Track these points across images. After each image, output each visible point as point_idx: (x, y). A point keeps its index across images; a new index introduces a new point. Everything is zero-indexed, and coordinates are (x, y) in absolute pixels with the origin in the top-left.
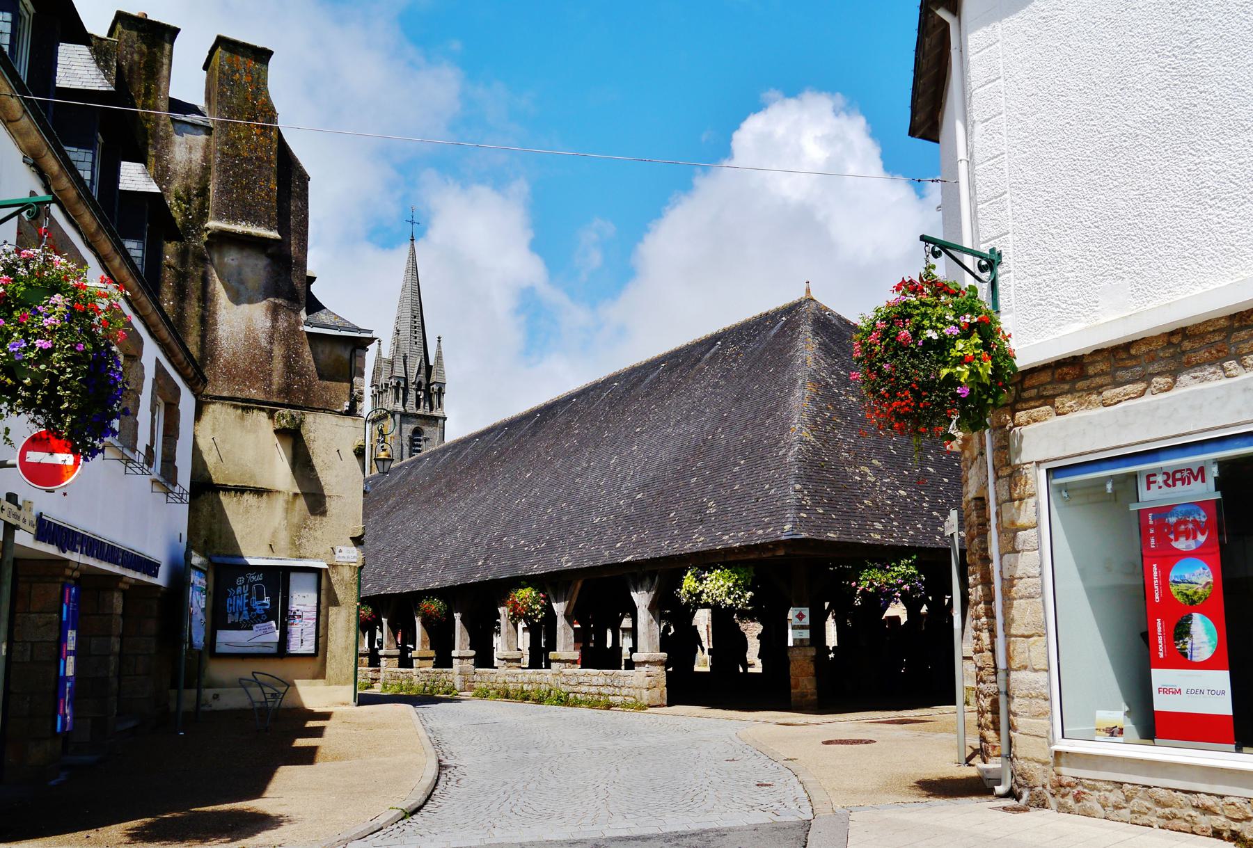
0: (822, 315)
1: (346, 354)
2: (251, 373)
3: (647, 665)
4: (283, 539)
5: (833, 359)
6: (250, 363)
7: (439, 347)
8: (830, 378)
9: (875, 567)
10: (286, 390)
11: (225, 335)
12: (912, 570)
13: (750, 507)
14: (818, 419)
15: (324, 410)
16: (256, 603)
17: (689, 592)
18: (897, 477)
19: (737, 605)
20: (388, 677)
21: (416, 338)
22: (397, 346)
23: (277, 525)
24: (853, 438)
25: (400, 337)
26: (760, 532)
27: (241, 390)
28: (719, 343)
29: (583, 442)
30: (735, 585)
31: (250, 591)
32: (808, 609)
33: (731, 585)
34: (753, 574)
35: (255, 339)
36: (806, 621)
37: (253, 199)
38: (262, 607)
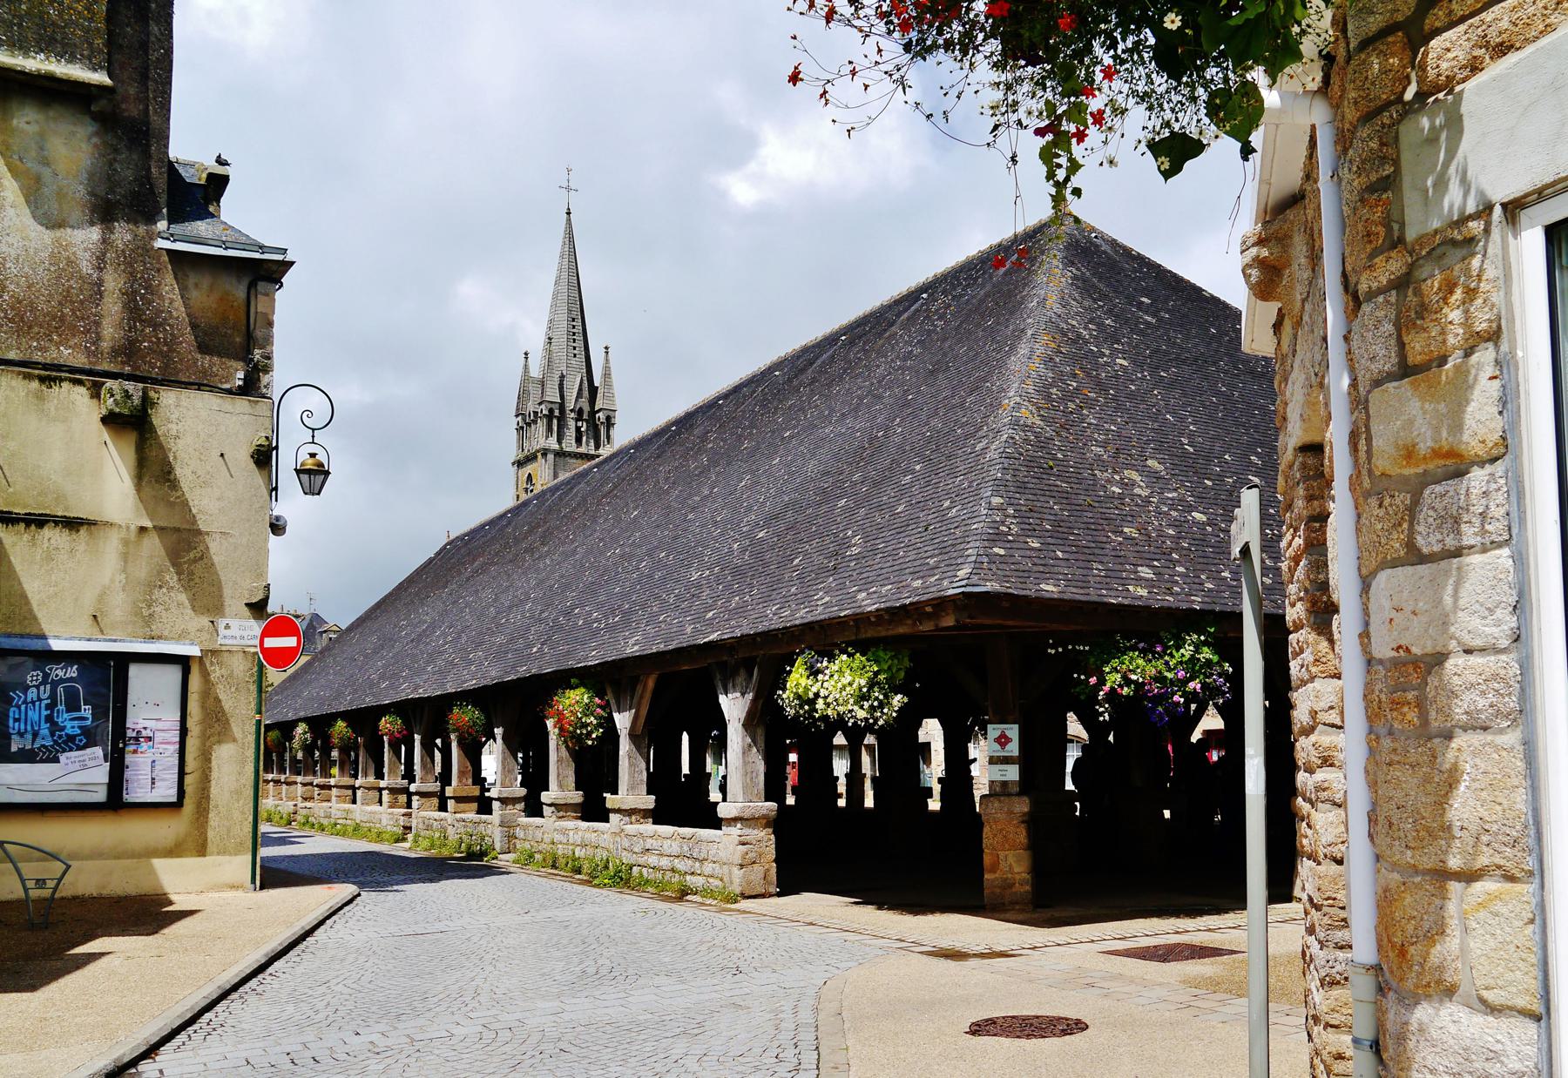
0: (1084, 237)
1: (240, 292)
2: (62, 319)
3: (739, 825)
4: (119, 606)
5: (1095, 300)
6: (60, 303)
7: (607, 360)
8: (1085, 329)
9: (1133, 648)
10: (128, 350)
11: (13, 253)
12: (1207, 654)
13: (913, 541)
14: (1054, 390)
15: (199, 386)
16: (65, 715)
17: (798, 697)
18: (1192, 490)
19: (876, 720)
21: (575, 348)
23: (106, 581)
24: (1115, 424)
25: (553, 348)
26: (917, 583)
27: (43, 349)
28: (925, 296)
29: (714, 462)
30: (872, 684)
31: (53, 696)
32: (1016, 727)
33: (863, 682)
34: (907, 663)
35: (70, 262)
36: (1013, 749)
37: (60, 15)
38: (76, 723)
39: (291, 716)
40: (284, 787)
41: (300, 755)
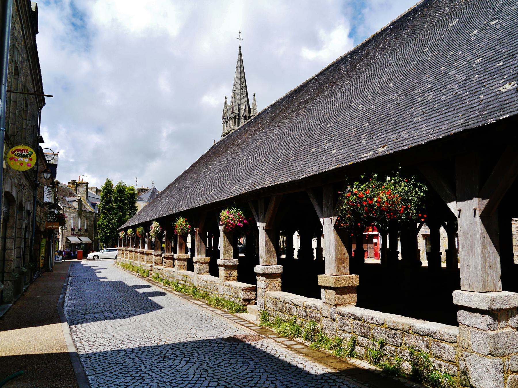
7: (254, 98)
20: (271, 305)
22: (234, 98)
39: (148, 219)
40: (145, 256)
41: (153, 239)
